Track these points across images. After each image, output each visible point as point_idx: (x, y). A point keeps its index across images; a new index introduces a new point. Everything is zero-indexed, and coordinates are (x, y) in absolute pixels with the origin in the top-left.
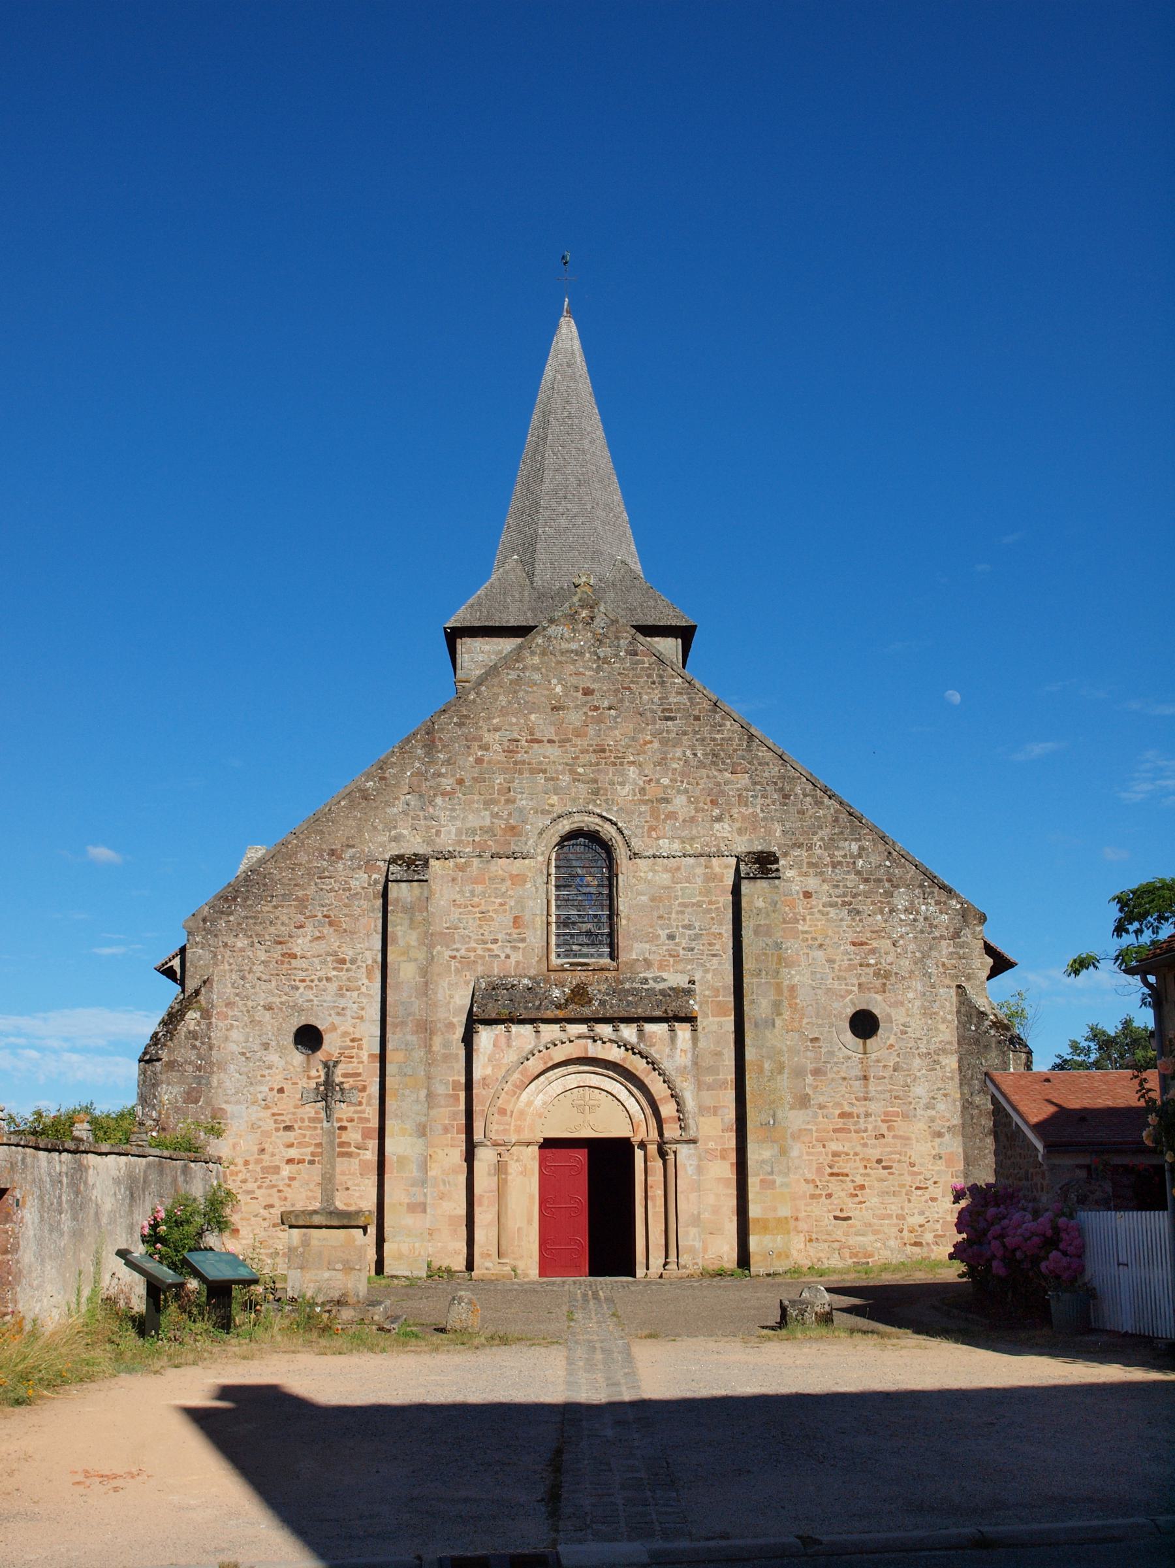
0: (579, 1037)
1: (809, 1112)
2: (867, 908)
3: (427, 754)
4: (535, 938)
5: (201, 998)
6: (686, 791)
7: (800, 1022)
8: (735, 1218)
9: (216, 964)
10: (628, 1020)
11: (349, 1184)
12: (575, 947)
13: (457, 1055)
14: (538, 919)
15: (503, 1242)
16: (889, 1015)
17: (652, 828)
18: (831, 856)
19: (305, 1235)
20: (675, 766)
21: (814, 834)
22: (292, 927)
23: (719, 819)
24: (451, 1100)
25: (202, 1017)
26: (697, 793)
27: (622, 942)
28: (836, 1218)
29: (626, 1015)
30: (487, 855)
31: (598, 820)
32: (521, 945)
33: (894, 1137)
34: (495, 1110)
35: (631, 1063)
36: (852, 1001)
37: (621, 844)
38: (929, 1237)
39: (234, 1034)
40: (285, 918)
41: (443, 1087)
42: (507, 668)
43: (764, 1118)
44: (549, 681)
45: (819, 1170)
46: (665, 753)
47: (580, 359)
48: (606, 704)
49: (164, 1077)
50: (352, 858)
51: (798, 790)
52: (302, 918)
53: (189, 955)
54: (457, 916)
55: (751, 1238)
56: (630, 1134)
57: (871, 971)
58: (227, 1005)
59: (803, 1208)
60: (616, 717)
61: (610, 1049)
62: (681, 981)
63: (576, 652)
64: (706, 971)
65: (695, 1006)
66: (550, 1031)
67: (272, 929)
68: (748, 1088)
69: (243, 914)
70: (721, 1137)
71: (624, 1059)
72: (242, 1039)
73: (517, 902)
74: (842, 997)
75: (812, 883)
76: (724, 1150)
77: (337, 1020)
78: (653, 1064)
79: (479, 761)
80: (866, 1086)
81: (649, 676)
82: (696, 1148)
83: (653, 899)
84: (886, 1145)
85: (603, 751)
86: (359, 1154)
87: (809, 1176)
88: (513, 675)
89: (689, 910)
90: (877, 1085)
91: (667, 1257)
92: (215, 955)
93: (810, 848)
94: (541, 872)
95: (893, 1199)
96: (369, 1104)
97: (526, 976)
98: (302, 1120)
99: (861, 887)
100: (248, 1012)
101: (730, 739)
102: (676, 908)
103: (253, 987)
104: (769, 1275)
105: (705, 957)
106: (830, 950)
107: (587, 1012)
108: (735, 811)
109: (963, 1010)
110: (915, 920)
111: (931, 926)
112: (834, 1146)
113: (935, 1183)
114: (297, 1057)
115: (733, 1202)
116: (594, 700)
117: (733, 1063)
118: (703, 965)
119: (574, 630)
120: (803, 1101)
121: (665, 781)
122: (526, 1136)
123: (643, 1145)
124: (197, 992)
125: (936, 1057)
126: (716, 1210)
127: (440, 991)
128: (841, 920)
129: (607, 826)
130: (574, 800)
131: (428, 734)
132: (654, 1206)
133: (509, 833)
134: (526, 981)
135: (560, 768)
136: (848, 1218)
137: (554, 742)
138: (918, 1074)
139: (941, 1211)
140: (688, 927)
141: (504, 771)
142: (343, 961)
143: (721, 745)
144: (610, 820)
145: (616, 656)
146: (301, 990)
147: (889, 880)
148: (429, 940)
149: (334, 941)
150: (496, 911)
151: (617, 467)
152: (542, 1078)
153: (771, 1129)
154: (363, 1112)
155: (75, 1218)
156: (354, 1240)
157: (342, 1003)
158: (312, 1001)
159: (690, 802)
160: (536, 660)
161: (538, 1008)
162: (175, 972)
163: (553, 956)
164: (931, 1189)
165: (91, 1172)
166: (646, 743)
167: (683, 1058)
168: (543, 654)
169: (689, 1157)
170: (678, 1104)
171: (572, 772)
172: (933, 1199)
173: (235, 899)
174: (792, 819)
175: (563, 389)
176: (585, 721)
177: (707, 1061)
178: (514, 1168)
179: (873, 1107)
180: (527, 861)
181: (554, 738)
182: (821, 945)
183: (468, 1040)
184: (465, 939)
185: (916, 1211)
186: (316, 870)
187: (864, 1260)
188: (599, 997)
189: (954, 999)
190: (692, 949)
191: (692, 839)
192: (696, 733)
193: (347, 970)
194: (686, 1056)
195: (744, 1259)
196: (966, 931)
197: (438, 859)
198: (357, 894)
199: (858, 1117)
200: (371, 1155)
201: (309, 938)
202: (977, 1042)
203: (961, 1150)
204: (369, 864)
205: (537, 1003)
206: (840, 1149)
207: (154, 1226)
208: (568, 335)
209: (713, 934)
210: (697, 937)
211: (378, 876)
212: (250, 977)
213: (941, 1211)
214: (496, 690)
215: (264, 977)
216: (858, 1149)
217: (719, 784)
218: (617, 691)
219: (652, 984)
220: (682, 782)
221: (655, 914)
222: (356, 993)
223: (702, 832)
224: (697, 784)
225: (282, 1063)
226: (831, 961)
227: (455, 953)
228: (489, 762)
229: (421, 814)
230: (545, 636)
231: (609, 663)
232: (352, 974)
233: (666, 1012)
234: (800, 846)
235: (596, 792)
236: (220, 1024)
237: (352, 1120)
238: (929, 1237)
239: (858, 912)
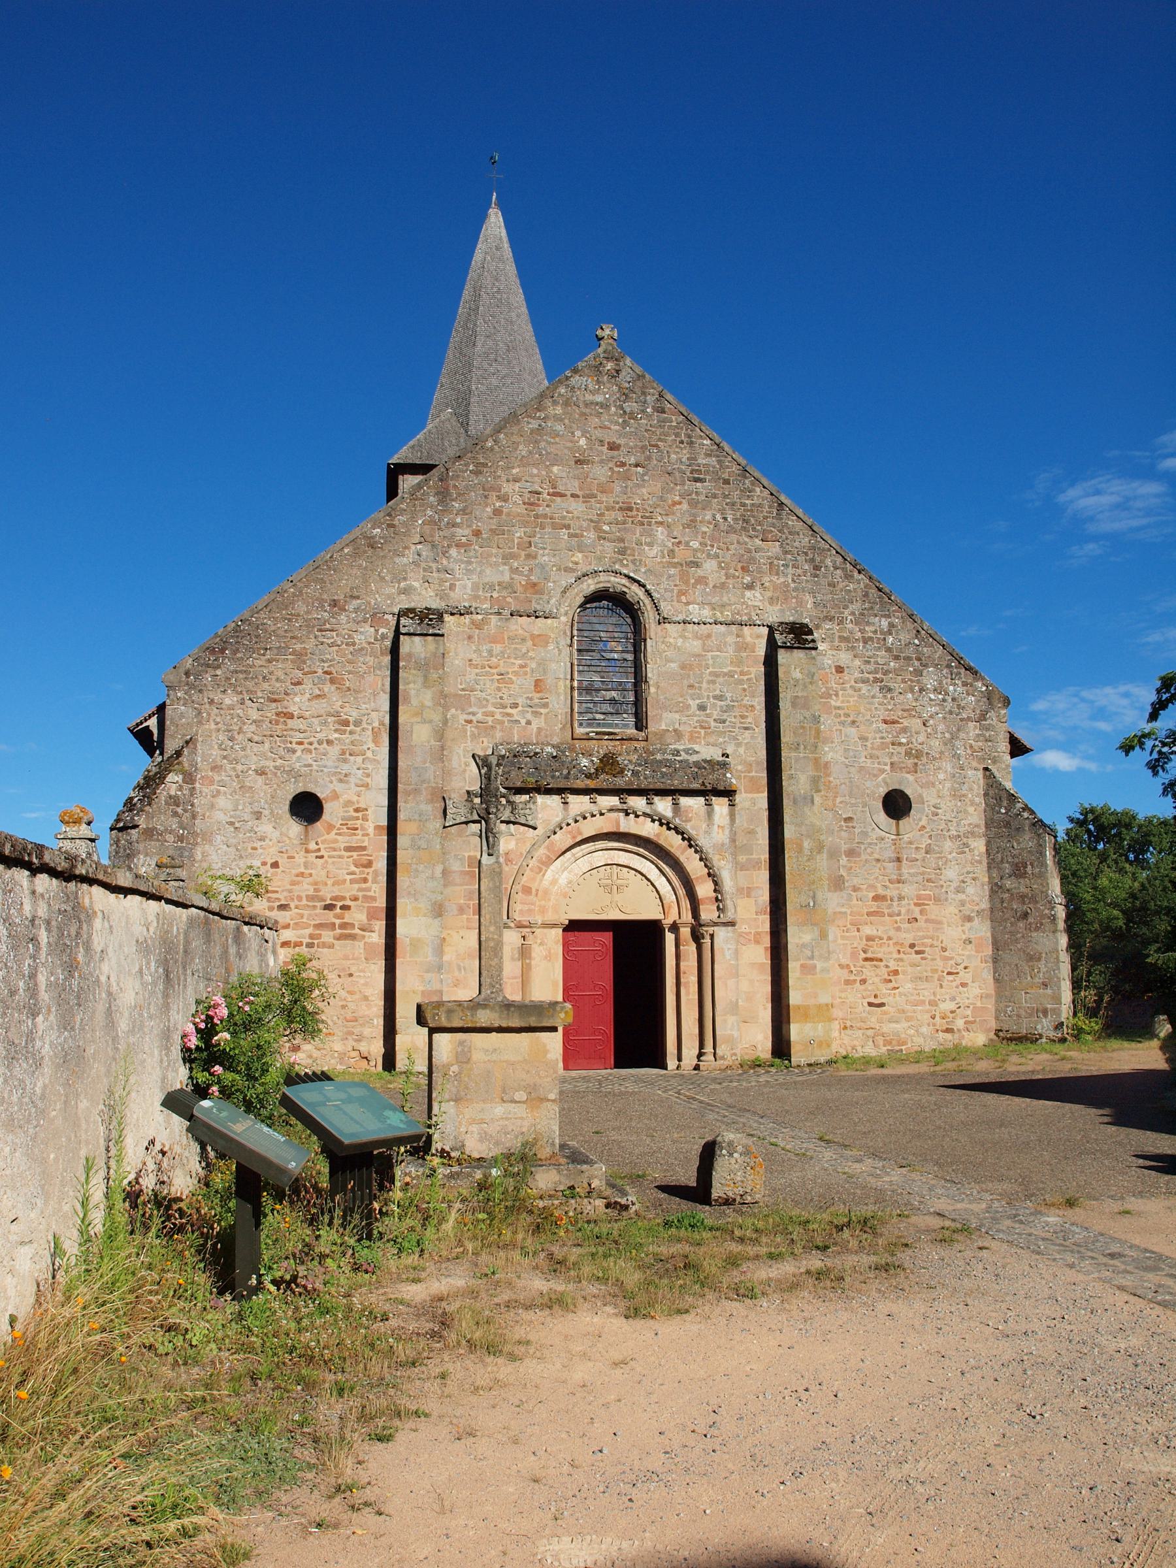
0: (610, 810)
1: (844, 894)
2: (898, 686)
3: (440, 502)
4: (559, 702)
5: (184, 759)
6: (717, 556)
7: (834, 800)
8: (769, 1005)
9: (200, 722)
10: (663, 793)
11: (353, 970)
12: (598, 716)
14: (561, 683)
16: (920, 796)
17: (682, 593)
18: (862, 631)
19: (461, 1043)
20: (705, 529)
21: (846, 607)
22: (288, 684)
23: (750, 587)
24: (467, 877)
25: (184, 781)
26: (728, 559)
28: (870, 1004)
29: (662, 787)
30: (507, 612)
31: (625, 581)
32: (542, 711)
33: (927, 921)
35: (666, 839)
36: (884, 780)
37: (649, 607)
38: (960, 1023)
39: (221, 802)
40: (280, 674)
41: (458, 863)
42: (528, 416)
43: (803, 899)
44: (573, 433)
45: (854, 955)
46: (695, 515)
47: (506, 245)
48: (633, 460)
49: (141, 847)
50: (356, 610)
51: (828, 562)
52: (300, 674)
53: (169, 711)
54: (473, 676)
55: (792, 1026)
56: (660, 916)
57: (902, 750)
58: (213, 769)
59: (838, 994)
60: (643, 475)
62: (715, 754)
63: (602, 405)
64: (739, 745)
65: (734, 781)
66: (579, 803)
67: (266, 686)
68: (787, 868)
69: (232, 668)
71: (658, 835)
72: (230, 807)
73: (539, 664)
74: (875, 776)
75: (844, 658)
76: (758, 933)
77: (339, 787)
78: (690, 841)
79: (497, 512)
80: (899, 869)
81: (677, 435)
82: (734, 932)
83: (683, 667)
84: (919, 929)
85: (630, 509)
86: (364, 937)
87: (844, 961)
88: (534, 424)
89: (721, 679)
90: (911, 867)
92: (200, 713)
93: (841, 623)
94: (565, 633)
95: (925, 985)
96: (375, 881)
97: (548, 744)
98: (300, 898)
99: (892, 664)
100: (238, 776)
101: (760, 505)
102: (707, 677)
103: (243, 749)
104: (810, 1065)
105: (737, 730)
106: (862, 727)
107: (620, 782)
108: (766, 579)
109: (991, 792)
110: (944, 700)
111: (959, 706)
112: (868, 930)
113: (965, 968)
114: (295, 828)
115: (767, 989)
116: (621, 455)
119: (598, 382)
120: (838, 883)
121: (695, 544)
122: (550, 917)
123: (674, 928)
124: (179, 753)
125: (965, 840)
127: (455, 758)
128: (873, 697)
129: (635, 587)
130: (600, 559)
131: (441, 480)
132: (688, 994)
133: (531, 591)
134: (549, 749)
135: (585, 524)
136: (882, 1005)
137: (578, 496)
138: (950, 857)
139: (971, 996)
140: (720, 698)
141: (525, 524)
142: (346, 723)
143: (752, 511)
144: (638, 582)
145: (643, 411)
146: (299, 753)
147: (919, 659)
148: (444, 700)
149: (336, 700)
151: (538, 341)
152: (568, 854)
153: (811, 909)
154: (369, 890)
155: (66, 1024)
156: (546, 1052)
157: (345, 768)
158: (310, 765)
159: (720, 567)
160: (559, 410)
161: (567, 777)
162: (151, 733)
164: (962, 974)
165: (98, 923)
166: (675, 504)
168: (567, 404)
170: (716, 883)
171: (598, 529)
172: (964, 985)
173: (222, 651)
174: (823, 591)
175: (492, 268)
176: (611, 477)
177: (741, 840)
178: (537, 952)
179: (908, 890)
180: (549, 621)
181: (578, 493)
182: (854, 722)
184: (482, 703)
185: (947, 997)
186: (316, 622)
187: (897, 1048)
188: (631, 767)
189: (982, 782)
191: (723, 606)
192: (726, 497)
193: (351, 733)
194: (726, 831)
195: (781, 1047)
196: (991, 714)
197: (452, 614)
198: (362, 649)
199: (892, 900)
200: (377, 938)
201: (307, 696)
202: (1008, 825)
203: (989, 934)
204: (376, 618)
205: (565, 772)
206: (875, 933)
207: (207, 1033)
208: (495, 223)
209: (745, 706)
210: (728, 709)
211: (387, 631)
212: (239, 738)
213: (971, 996)
214: (515, 438)
215: (256, 738)
216: (892, 933)
217: (749, 551)
218: (643, 448)
219: (684, 756)
220: (712, 546)
221: (685, 682)
222: (359, 759)
223: (733, 600)
224: (728, 549)
225: (276, 834)
226: (863, 739)
227: (471, 717)
228: (508, 514)
229: (434, 566)
230: (567, 386)
231: (635, 418)
232: (356, 737)
234: (831, 619)
235: (622, 552)
236: (205, 790)
237: (356, 899)
238: (960, 1023)
239: (890, 690)
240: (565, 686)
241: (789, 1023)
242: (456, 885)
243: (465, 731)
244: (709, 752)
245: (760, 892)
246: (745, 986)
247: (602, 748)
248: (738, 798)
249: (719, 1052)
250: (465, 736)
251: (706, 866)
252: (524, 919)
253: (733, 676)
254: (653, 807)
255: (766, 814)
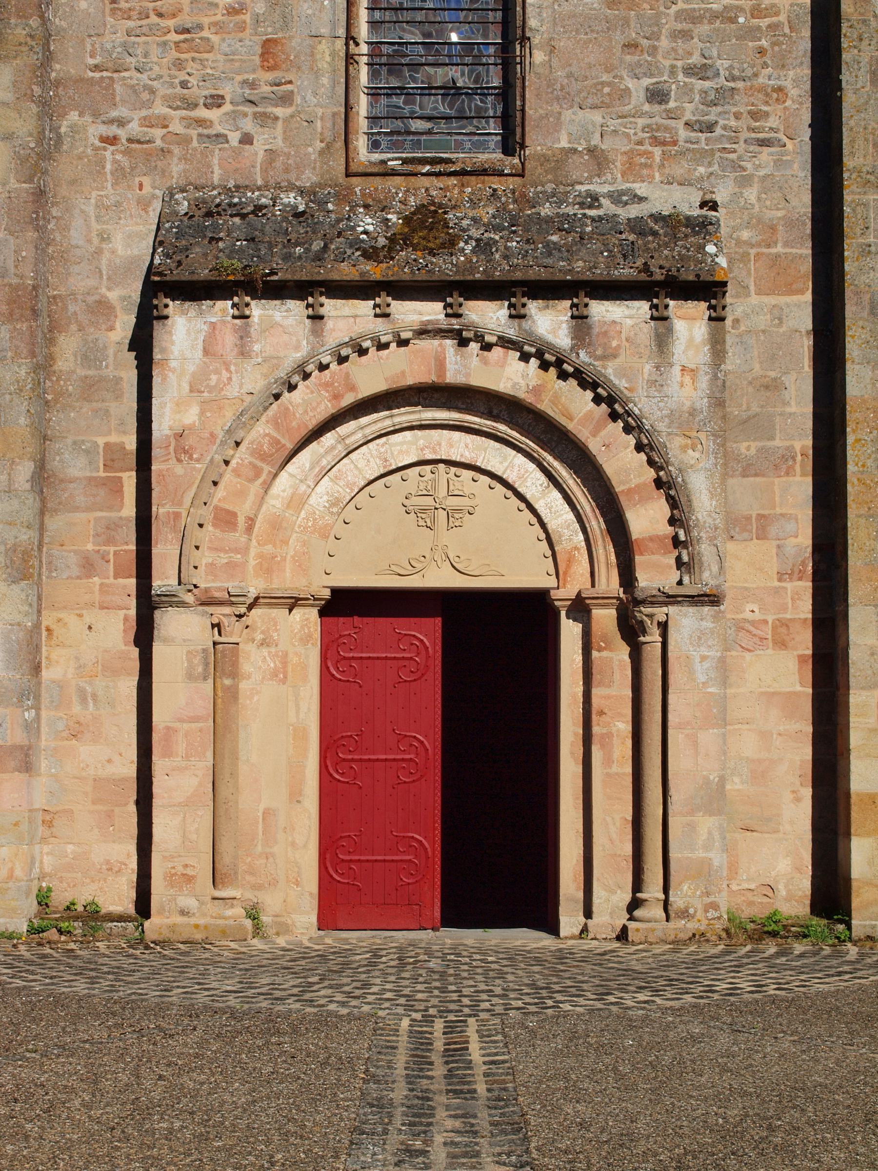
4: (316, 94)
10: (548, 290)
13: (118, 380)
14: (324, 47)
15: (226, 846)
24: (102, 492)
27: (535, 106)
32: (279, 111)
34: (205, 514)
41: (82, 461)
54: (120, 37)
56: (550, 582)
61: (502, 364)
62: (686, 202)
64: (745, 181)
65: (719, 257)
66: (348, 317)
68: (851, 468)
70: (776, 591)
71: (537, 391)
76: (783, 623)
78: (613, 405)
82: (716, 618)
89: (704, 28)
91: (638, 884)
97: (291, 187)
102: (669, 24)
105: (741, 147)
107: (444, 266)
117: (809, 409)
118: (736, 166)
122: (288, 581)
123: (580, 608)
126: (760, 773)
127: (77, 223)
132: (608, 761)
140: (701, 71)
150: (218, 27)
152: (329, 439)
161: (319, 258)
163: (361, 144)
167: (688, 390)
169: (699, 638)
170: (673, 503)
178: (255, 661)
183: (142, 344)
184: (142, 96)
188: (475, 233)
190: (710, 127)
209: (762, 89)
210: (722, 96)
219: (607, 207)
221: (619, 38)
227: (113, 130)
233: (646, 268)
240: (333, 54)
241: (848, 835)
242: (77, 509)
243: (101, 163)
244: (666, 196)
245: (790, 527)
246: (747, 745)
247: (409, 194)
248: (735, 305)
249: (677, 900)
250: (101, 173)
251: (651, 462)
252: (216, 585)
253: (733, 20)
254: (526, 324)
255: (808, 343)
